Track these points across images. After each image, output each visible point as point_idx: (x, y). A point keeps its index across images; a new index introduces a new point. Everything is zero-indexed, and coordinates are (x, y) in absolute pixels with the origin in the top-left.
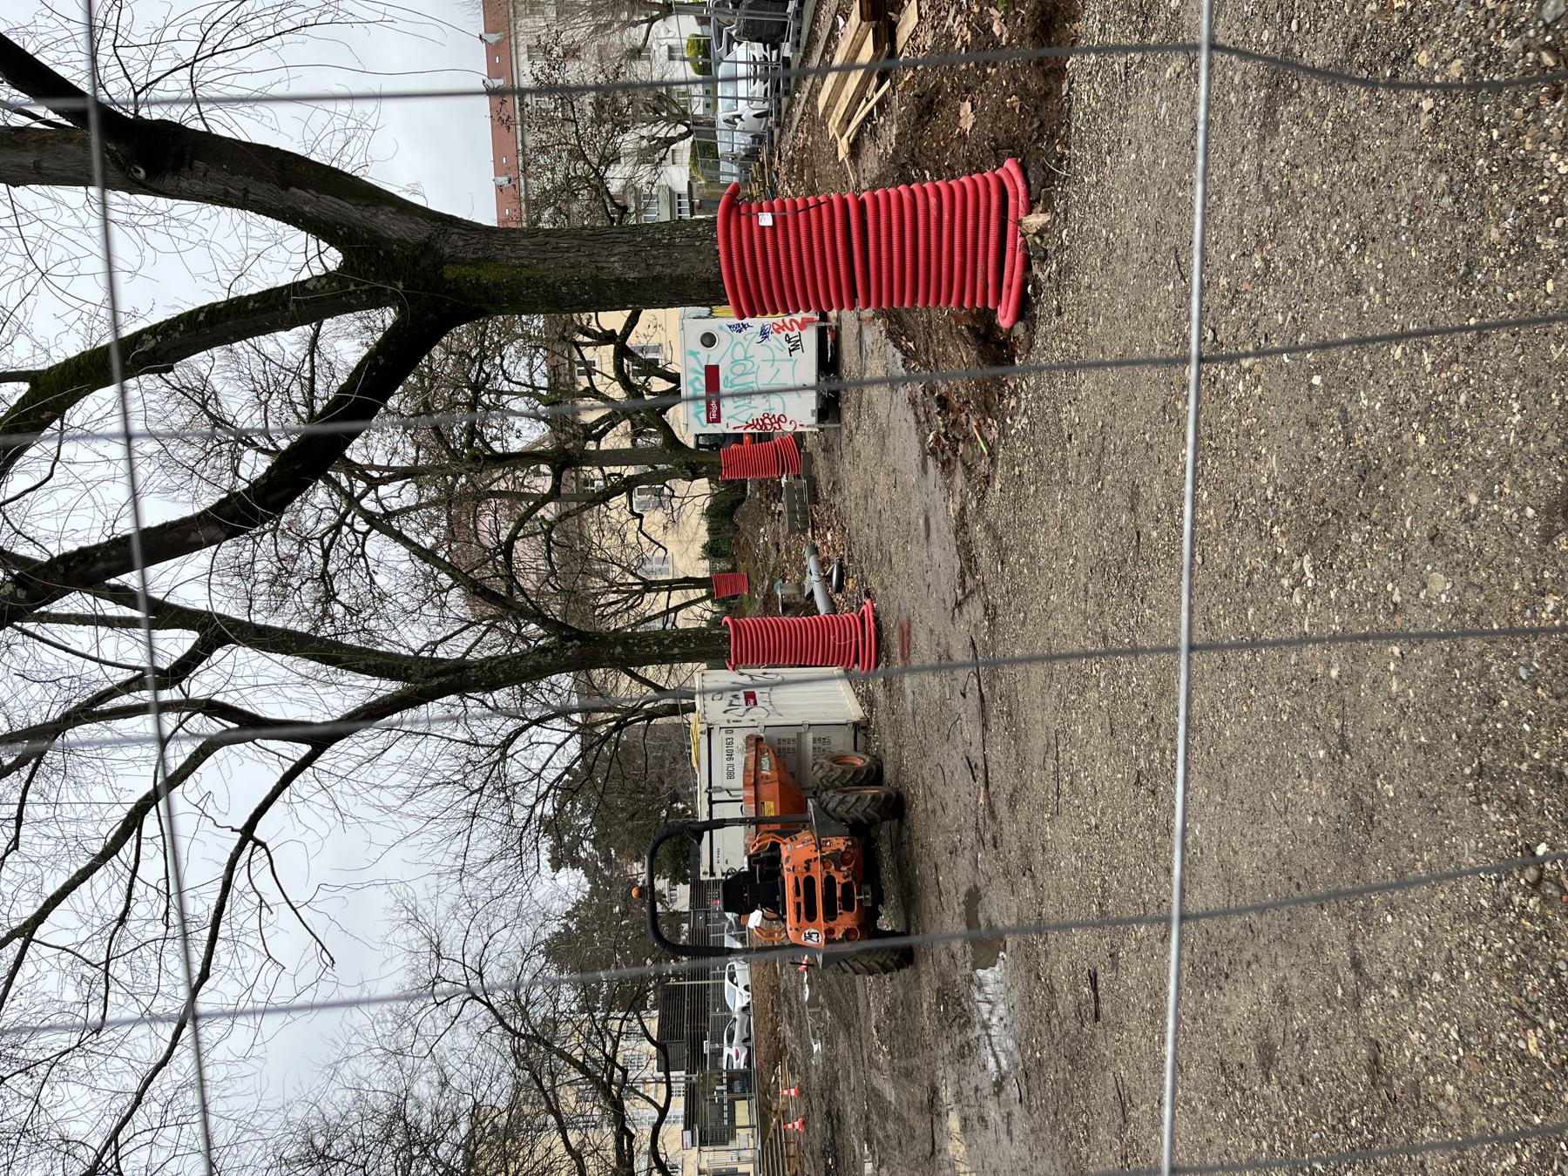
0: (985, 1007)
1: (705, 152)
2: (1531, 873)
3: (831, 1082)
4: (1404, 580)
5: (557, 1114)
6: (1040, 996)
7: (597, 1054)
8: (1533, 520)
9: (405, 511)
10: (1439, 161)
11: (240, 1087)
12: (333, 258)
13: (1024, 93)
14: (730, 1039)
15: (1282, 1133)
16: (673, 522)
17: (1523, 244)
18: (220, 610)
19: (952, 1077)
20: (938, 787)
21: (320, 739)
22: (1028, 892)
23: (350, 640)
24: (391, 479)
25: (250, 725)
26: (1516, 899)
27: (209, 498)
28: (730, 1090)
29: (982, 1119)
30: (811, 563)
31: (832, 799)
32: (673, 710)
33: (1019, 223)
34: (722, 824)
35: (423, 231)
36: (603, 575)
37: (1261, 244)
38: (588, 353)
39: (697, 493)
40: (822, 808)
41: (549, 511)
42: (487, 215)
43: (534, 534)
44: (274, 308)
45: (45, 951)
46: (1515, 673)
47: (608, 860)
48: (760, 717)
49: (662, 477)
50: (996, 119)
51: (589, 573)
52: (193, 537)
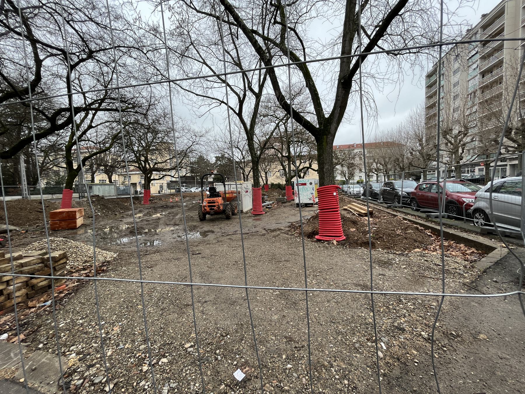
0: (192, 234)
1: (344, 183)
2: (224, 334)
3: (179, 207)
4: (276, 311)
5: (172, 158)
6: (196, 244)
7: (183, 165)
8: (288, 335)
9: (279, 130)
10: (353, 317)
11: (178, 101)
12: (327, 116)
13: (357, 240)
14: (186, 189)
15: (175, 288)
16: (278, 177)
17: (339, 333)
18: (262, 97)
19: (181, 228)
20: (232, 226)
21: (240, 114)
22: (214, 242)
23: (257, 120)
24: (285, 127)
25: (241, 102)
26: (219, 332)
27: (283, 93)
28: (177, 189)
29: (174, 233)
30: (271, 202)
31: (229, 207)
32: (244, 178)
33: (334, 239)
34: (225, 187)
35: (332, 132)
36: (268, 165)
37: (335, 284)
38: (308, 162)
39: (283, 182)
40: (228, 205)
41: (280, 155)
42: (335, 144)
43: (275, 153)
44: (318, 105)
45: (201, 66)
46: (260, 331)
47: (217, 166)
48: (243, 193)
49: (286, 175)
50: (353, 235)
51: (268, 163)
52: (277, 91)
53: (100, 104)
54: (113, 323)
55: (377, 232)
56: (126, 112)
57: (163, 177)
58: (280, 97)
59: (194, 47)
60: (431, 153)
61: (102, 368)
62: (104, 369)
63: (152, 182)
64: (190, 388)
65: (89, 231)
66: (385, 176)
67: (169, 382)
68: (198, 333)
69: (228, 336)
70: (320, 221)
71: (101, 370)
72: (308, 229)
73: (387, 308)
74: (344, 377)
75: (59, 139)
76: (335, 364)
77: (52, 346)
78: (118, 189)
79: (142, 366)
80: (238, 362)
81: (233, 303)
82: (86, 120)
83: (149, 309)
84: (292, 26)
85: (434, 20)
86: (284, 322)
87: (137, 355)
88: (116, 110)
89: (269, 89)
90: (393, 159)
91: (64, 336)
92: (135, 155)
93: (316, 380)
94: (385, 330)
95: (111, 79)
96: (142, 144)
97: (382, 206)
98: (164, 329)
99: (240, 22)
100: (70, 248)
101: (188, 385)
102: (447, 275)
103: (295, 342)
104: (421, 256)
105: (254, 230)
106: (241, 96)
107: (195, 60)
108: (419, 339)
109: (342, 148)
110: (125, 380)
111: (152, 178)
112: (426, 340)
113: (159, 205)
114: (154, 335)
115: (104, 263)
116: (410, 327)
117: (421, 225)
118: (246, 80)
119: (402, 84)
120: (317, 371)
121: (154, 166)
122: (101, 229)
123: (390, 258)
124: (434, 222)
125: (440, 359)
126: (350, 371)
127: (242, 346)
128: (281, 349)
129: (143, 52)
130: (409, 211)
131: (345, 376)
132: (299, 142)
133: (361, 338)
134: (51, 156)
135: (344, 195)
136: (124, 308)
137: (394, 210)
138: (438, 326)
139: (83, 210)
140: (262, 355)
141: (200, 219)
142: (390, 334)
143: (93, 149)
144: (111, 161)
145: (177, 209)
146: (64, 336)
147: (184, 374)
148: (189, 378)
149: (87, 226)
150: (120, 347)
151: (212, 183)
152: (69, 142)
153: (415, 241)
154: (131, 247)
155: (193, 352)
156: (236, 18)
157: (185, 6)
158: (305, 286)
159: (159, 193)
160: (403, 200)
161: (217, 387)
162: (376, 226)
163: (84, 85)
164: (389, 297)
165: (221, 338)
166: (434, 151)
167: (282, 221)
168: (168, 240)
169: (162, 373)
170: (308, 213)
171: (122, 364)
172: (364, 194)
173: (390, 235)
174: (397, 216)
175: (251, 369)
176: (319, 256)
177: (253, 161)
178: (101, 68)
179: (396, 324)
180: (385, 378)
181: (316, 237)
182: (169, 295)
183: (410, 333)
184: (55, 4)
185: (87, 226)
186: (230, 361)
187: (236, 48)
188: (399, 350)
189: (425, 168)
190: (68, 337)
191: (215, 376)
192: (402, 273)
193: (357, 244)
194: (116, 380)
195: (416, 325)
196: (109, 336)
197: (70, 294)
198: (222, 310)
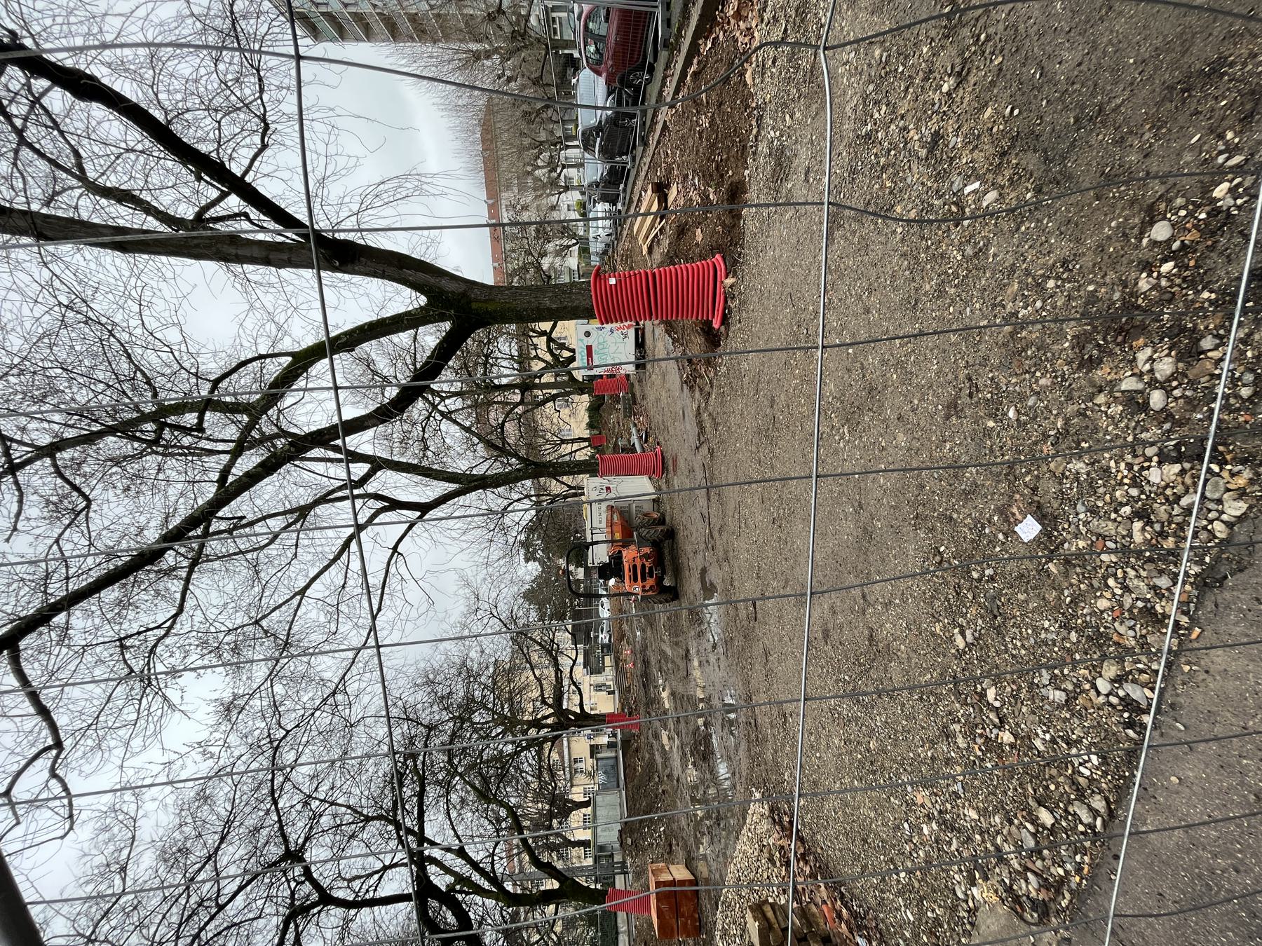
0: (708, 616)
1: (584, 251)
2: (938, 558)
5: (530, 663)
9: (457, 410)
10: (904, 255)
11: (397, 655)
12: (423, 300)
13: (724, 225)
14: (602, 631)
16: (573, 414)
17: (940, 291)
19: (695, 645)
20: (689, 526)
23: (436, 467)
25: (395, 505)
27: (372, 407)
28: (602, 652)
29: (707, 661)
30: (634, 430)
31: (644, 532)
32: (575, 495)
33: (722, 282)
34: (597, 543)
35: (463, 287)
36: (543, 437)
38: (535, 340)
39: (583, 401)
40: (639, 535)
41: (520, 410)
42: (489, 280)
44: (398, 322)
45: (310, 601)
47: (549, 558)
49: (568, 394)
51: (539, 436)
52: (366, 424)
53: (409, 831)
54: (908, 805)
55: (706, 177)
56: (424, 772)
57: (574, 684)
58: (383, 415)
59: (264, 617)
60: (508, 29)
61: (1005, 832)
62: (1007, 828)
64: (1054, 641)
66: (568, 147)
67: (1037, 685)
68: (934, 617)
69: (942, 549)
70: (677, 316)
72: (697, 344)
74: (1039, 286)
75: (490, 921)
76: (1009, 307)
77: (954, 936)
78: (604, 788)
79: (1001, 743)
80: (1001, 531)
81: (868, 534)
82: (446, 863)
83: (879, 724)
84: (208, 386)
85: (176, 28)
86: (913, 418)
87: (979, 753)
88: (421, 795)
90: (523, 126)
91: (933, 911)
92: (524, 749)
93: (1044, 354)
95: (349, 807)
96: (498, 735)
97: (641, 158)
98: (922, 693)
99: (202, 512)
100: (740, 895)
101: (1047, 645)
102: (809, 12)
104: (763, 74)
105: (699, 474)
106: (379, 504)
107: (295, 615)
108: (958, 99)
109: (501, 257)
110: (1031, 782)
111: (578, 711)
112: (961, 82)
113: (642, 692)
114: (935, 714)
115: (774, 820)
116: (931, 118)
117: (688, 63)
119: (338, 111)
120: (1024, 350)
121: (550, 706)
122: (698, 823)
123: (766, 151)
124: (679, 30)
125: (1006, 52)
127: (964, 518)
128: (974, 430)
129: (284, 737)
131: (1038, 285)
132: (485, 364)
133: (953, 240)
134: (529, 937)
135: (613, 252)
136: (876, 780)
138: (929, 50)
139: (654, 866)
140: (986, 475)
142: (945, 169)
144: (540, 805)
145: (649, 652)
146: (933, 911)
147: (1023, 652)
148: (1032, 641)
149: (689, 856)
150: (961, 791)
151: (588, 571)
153: (727, 80)
154: (737, 758)
155: (976, 631)
156: (194, 521)
157: (168, 641)
158: (807, 480)
159: (612, 693)
161: (1053, 580)
162: (690, 177)
163: (363, 868)
164: (860, 163)
169: (1019, 701)
170: (659, 341)
171: (996, 788)
172: (613, 202)
173: (713, 145)
174: (665, 122)
175: (1016, 501)
176: (763, 325)
177: (535, 476)
178: (323, 831)
179: (923, 153)
180: (1045, 189)
181: (716, 325)
182: (847, 678)
183: (943, 120)
184: (178, 937)
185: (689, 856)
186: (998, 549)
187: (264, 518)
188: (981, 151)
189: (547, 45)
191: (1028, 583)
193: (734, 226)
194: (1030, 801)
195: (925, 103)
196: (936, 814)
197: (842, 896)
198: (883, 560)
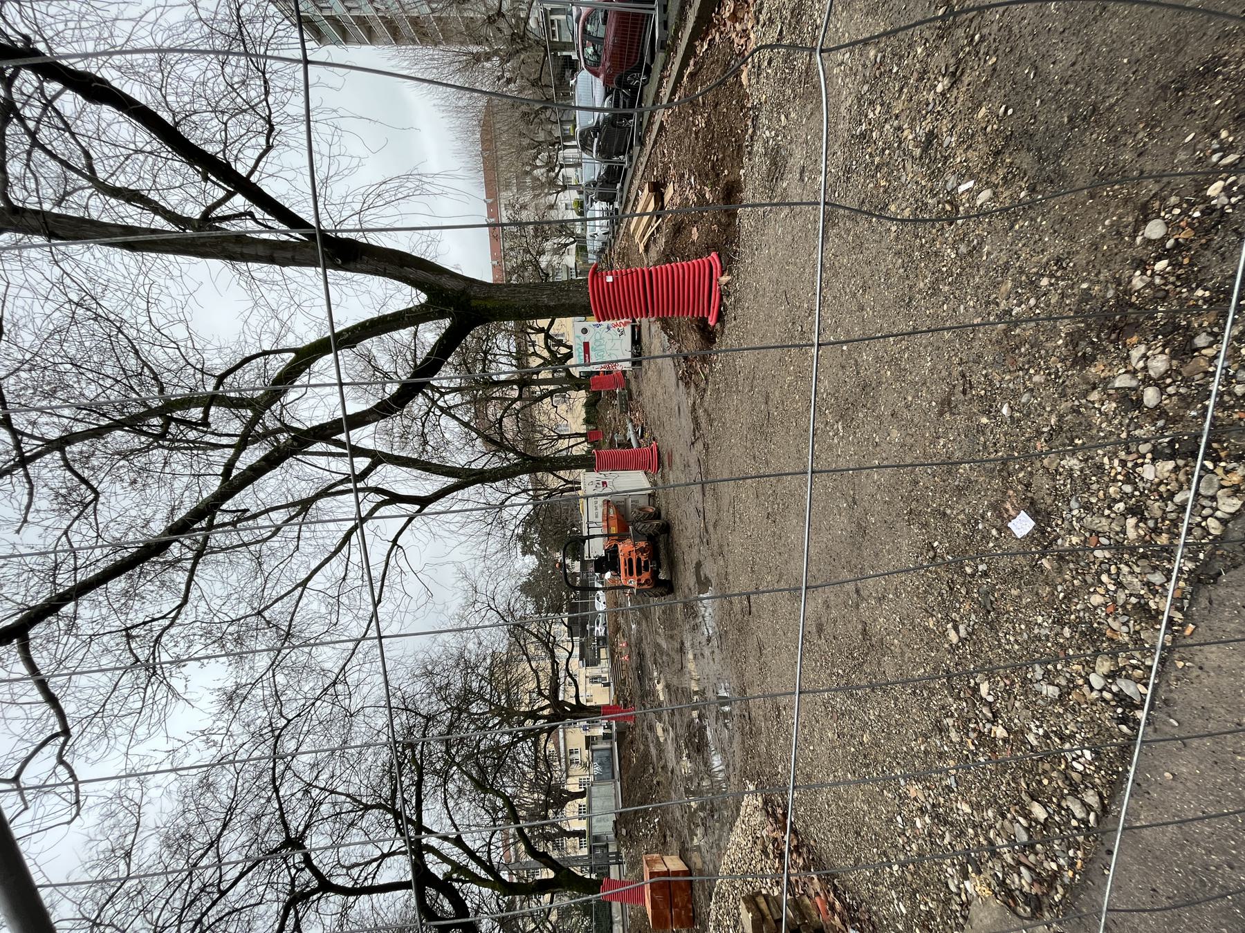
1: (582, 249)
2: (931, 554)
3: (640, 641)
4: (880, 432)
9: (456, 406)
10: (898, 253)
12: (423, 298)
13: (719, 223)
16: (570, 409)
20: (684, 520)
22: (721, 563)
23: (435, 461)
25: (395, 498)
30: (630, 426)
31: (640, 526)
32: (572, 489)
34: (593, 537)
35: (462, 285)
38: (533, 337)
39: (581, 396)
40: (635, 529)
41: (517, 405)
42: (488, 278)
47: (546, 552)
49: (565, 390)
51: (535, 431)
55: (702, 176)
57: (570, 675)
58: (384, 410)
59: (267, 608)
60: (507, 32)
61: (998, 826)
63: (583, 701)
64: (1047, 636)
65: (696, 841)
66: (566, 147)
69: (936, 544)
71: (1002, 827)
72: (692, 341)
73: (878, 168)
74: (1033, 284)
76: (1003, 305)
78: (599, 779)
84: (213, 381)
87: (972, 748)
88: (419, 784)
89: (363, 437)
90: (522, 127)
91: (926, 904)
92: (520, 739)
93: (1038, 352)
94: (930, 180)
95: (348, 795)
96: (495, 726)
98: (916, 688)
101: (1040, 640)
103: (951, 393)
105: (695, 469)
106: (379, 498)
108: (952, 99)
109: (499, 255)
110: (1024, 776)
111: (574, 702)
113: (637, 685)
114: (928, 708)
115: (767, 812)
116: (925, 117)
117: (684, 64)
118: (341, 488)
119: (341, 112)
120: (1018, 347)
121: (546, 697)
123: (762, 150)
124: (676, 32)
125: (1000, 52)
126: (1021, 271)
129: (286, 726)
130: (650, 90)
131: (1032, 282)
132: (485, 359)
134: (525, 926)
136: (869, 773)
137: (649, 129)
139: (649, 857)
141: (668, 593)
143: (507, 834)
145: (644, 645)
146: (926, 904)
147: (1016, 647)
148: (1025, 636)
150: (954, 785)
151: (584, 565)
152: (493, 888)
153: (723, 82)
156: (198, 514)
157: (173, 631)
159: (608, 685)
160: (624, 107)
163: (362, 856)
165: (939, 561)
166: (503, 24)
167: (675, 402)
168: (716, 667)
170: (655, 339)
171: (989, 782)
172: (610, 200)
176: (758, 322)
177: (532, 470)
179: (917, 152)
180: (1039, 188)
181: (711, 323)
184: (181, 922)
186: (991, 545)
187: (267, 511)
189: (545, 47)
190: (928, 895)
191: (1021, 578)
192: (798, 123)
194: (1023, 795)
195: (919, 103)
197: (835, 889)
198: (877, 555)
